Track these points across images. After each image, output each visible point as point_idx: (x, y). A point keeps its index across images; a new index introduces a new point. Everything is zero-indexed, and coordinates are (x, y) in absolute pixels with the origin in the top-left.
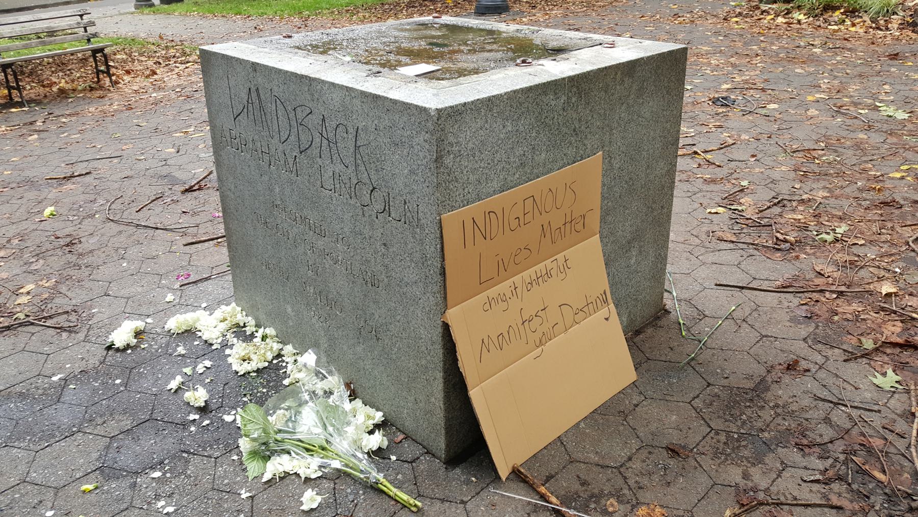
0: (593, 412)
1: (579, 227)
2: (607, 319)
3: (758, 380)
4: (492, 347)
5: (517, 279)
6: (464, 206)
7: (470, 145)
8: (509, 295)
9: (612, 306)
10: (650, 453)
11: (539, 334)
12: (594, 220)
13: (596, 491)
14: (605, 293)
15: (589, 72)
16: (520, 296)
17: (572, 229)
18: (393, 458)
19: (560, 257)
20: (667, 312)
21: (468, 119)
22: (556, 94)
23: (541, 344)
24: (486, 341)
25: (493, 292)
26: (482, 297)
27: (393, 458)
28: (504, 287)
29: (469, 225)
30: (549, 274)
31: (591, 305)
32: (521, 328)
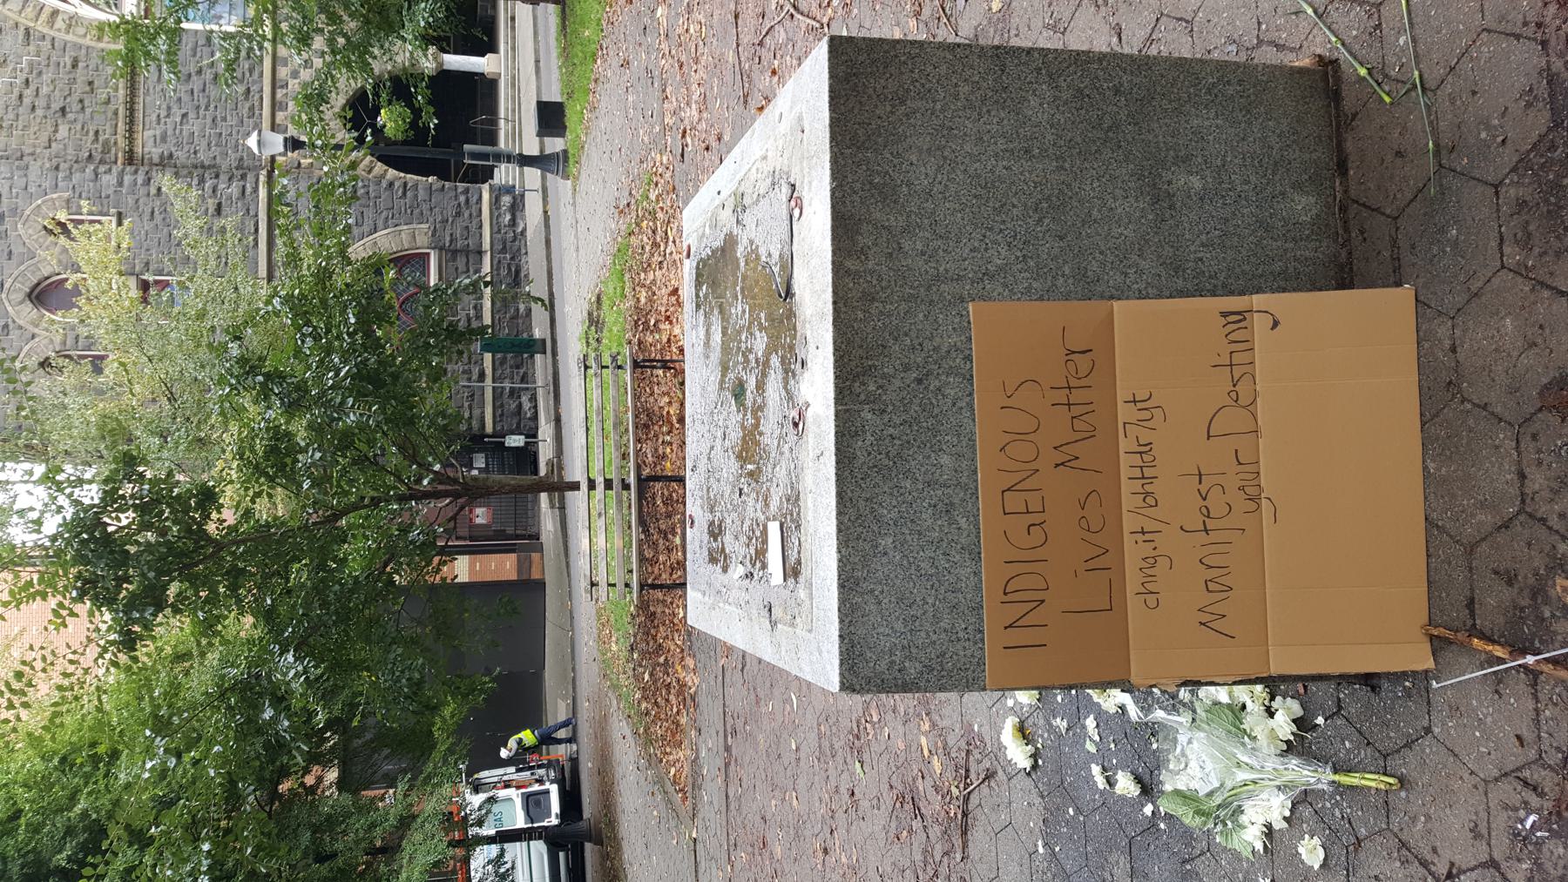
0: (1423, 424)
1: (1083, 362)
2: (1276, 324)
3: (1542, 89)
4: (1219, 609)
5: (1129, 523)
6: (982, 640)
7: (899, 626)
8: (1147, 550)
9: (1258, 300)
10: (1534, 437)
11: (1240, 503)
12: (1080, 314)
13: (1531, 580)
14: (1224, 315)
15: (836, 350)
16: (1159, 526)
17: (1087, 363)
18: (1320, 720)
19: (1124, 412)
20: (1328, 67)
21: (861, 631)
22: (856, 433)
23: (1254, 499)
24: (1205, 618)
25: (1133, 582)
26: (1133, 604)
27: (1320, 720)
28: (1133, 553)
29: (1016, 637)
30: (1144, 449)
31: (1237, 358)
32: (1213, 537)
